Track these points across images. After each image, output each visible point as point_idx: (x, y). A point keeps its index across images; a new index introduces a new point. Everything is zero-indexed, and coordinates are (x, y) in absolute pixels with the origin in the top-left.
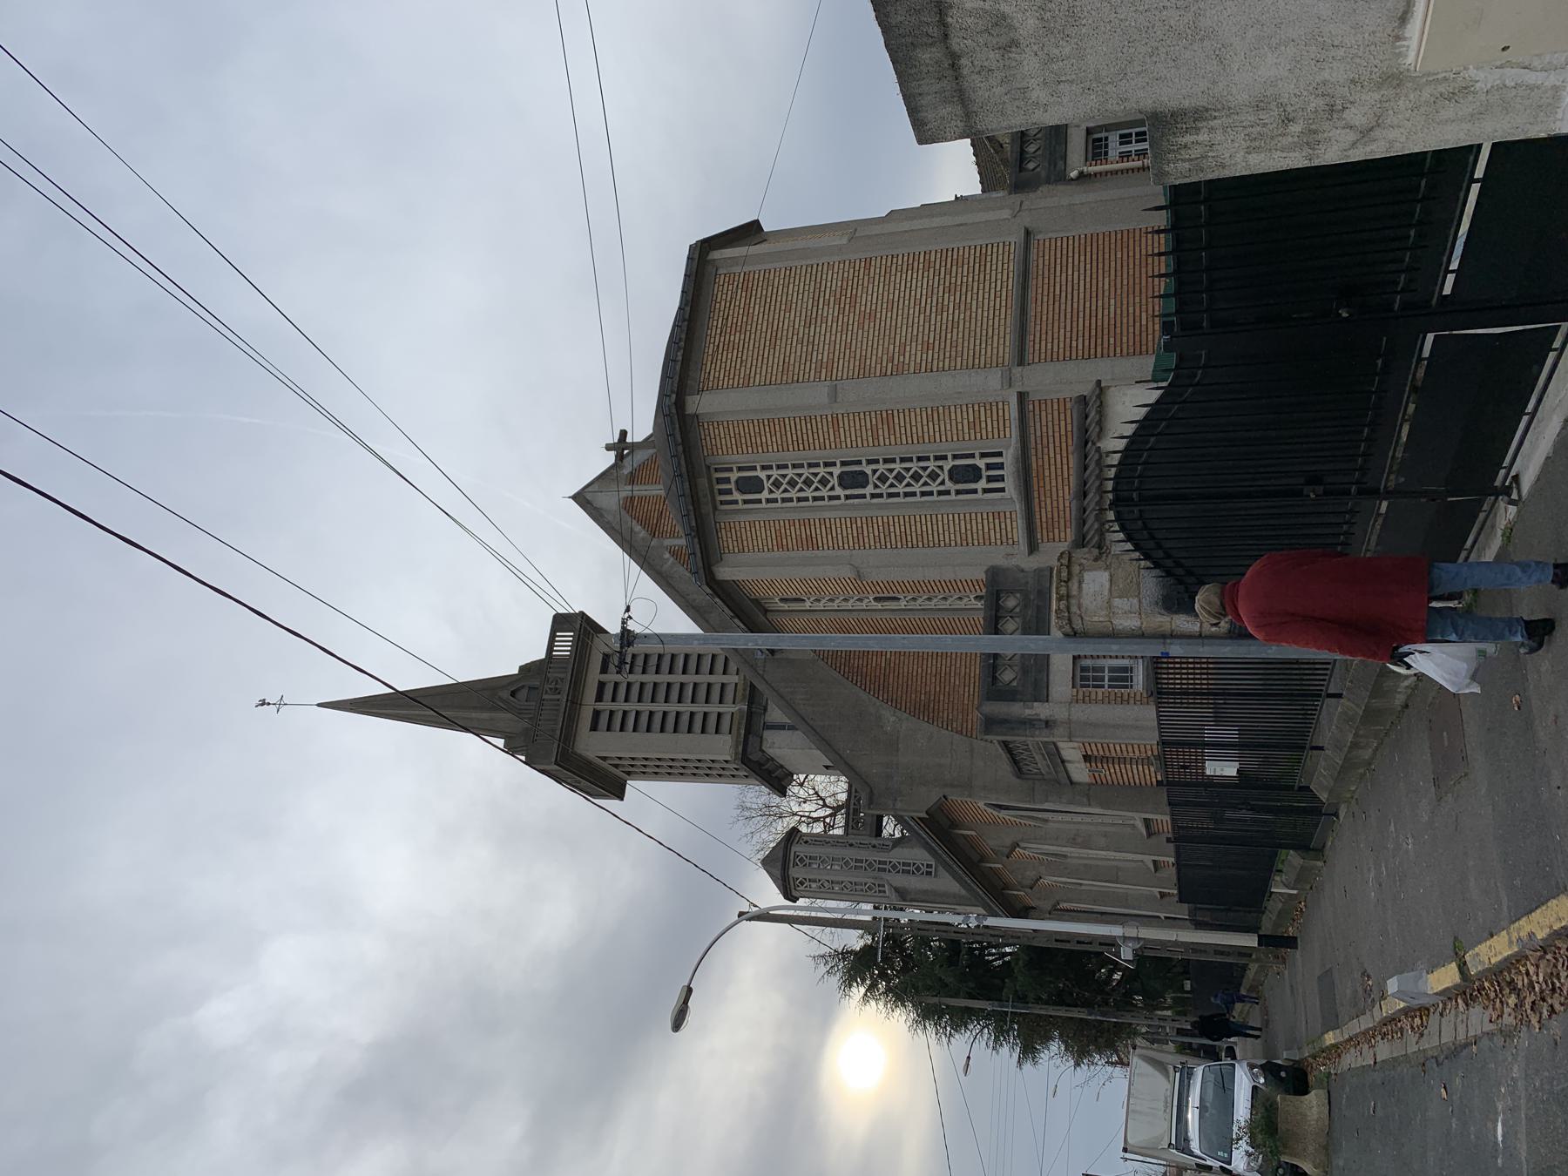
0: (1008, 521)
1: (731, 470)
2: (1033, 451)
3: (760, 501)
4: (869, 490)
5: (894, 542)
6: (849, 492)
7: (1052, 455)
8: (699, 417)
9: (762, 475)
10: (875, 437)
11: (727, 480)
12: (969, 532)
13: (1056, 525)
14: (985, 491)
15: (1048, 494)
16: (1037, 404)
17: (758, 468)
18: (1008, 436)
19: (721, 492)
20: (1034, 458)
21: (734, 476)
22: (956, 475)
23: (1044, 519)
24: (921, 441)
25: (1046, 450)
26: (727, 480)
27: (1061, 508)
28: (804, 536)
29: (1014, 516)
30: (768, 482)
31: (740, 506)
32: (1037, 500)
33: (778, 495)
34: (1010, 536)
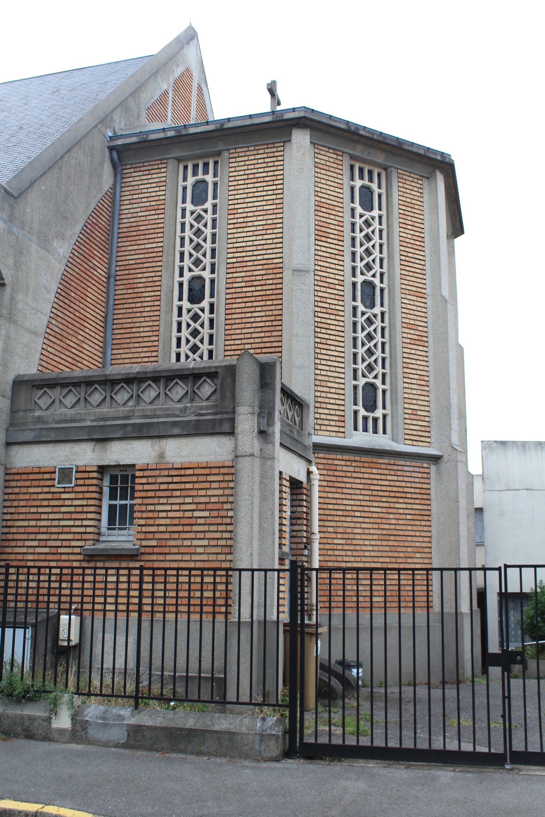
0: (336, 429)
1: (215, 175)
2: (392, 462)
3: (184, 201)
4: (186, 304)
5: (320, 315)
6: (359, 287)
7: (389, 478)
8: (426, 180)
9: (208, 205)
10: (409, 326)
11: (371, 180)
12: (327, 390)
13: (331, 473)
14: (356, 413)
15: (357, 469)
16: (427, 471)
17: (215, 201)
18: (407, 442)
19: (196, 167)
20: (386, 461)
21: (209, 178)
22: (371, 388)
23: (336, 462)
24: (405, 365)
25: (392, 473)
26: (206, 172)
27: (346, 480)
28: (329, 230)
29: (341, 435)
30: (200, 209)
31: (181, 183)
32: (352, 458)
33: (189, 219)
34: (323, 428)
